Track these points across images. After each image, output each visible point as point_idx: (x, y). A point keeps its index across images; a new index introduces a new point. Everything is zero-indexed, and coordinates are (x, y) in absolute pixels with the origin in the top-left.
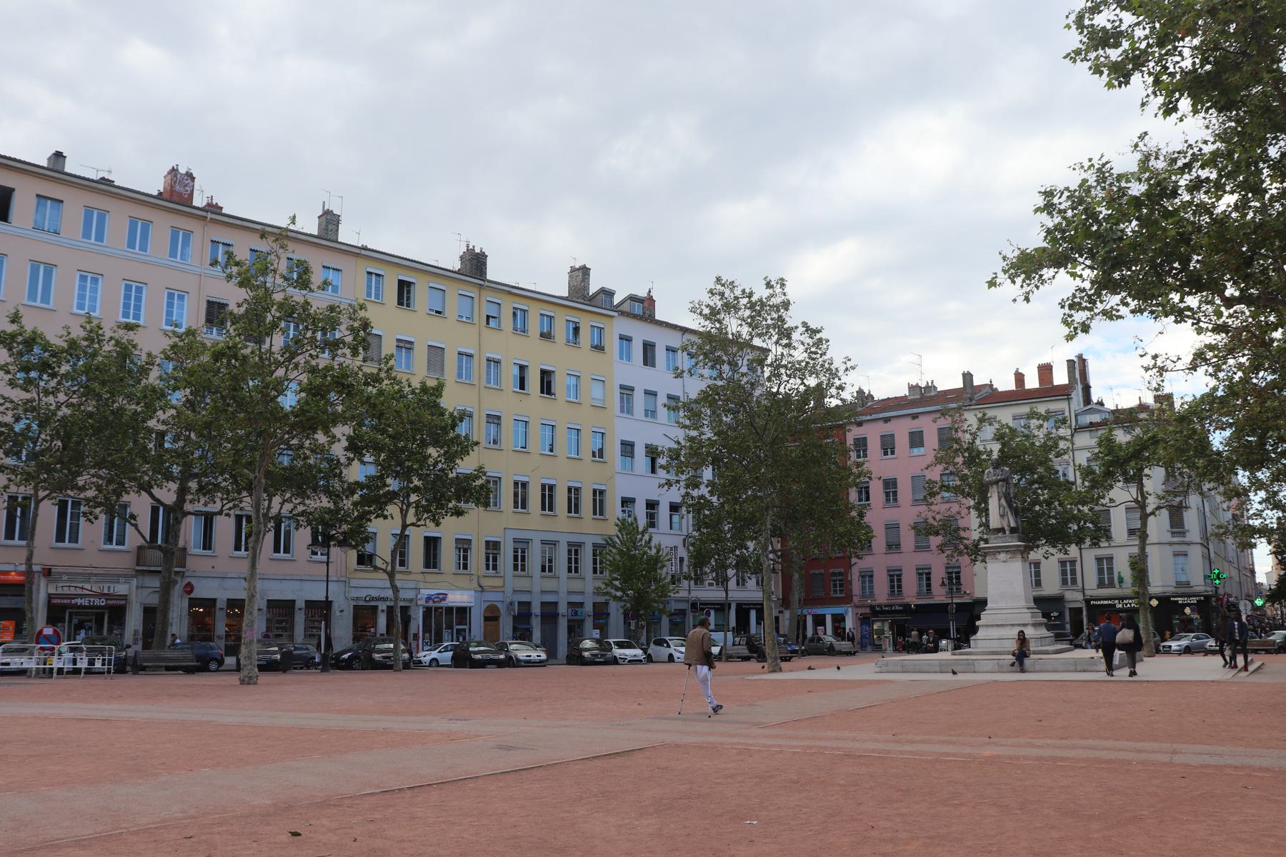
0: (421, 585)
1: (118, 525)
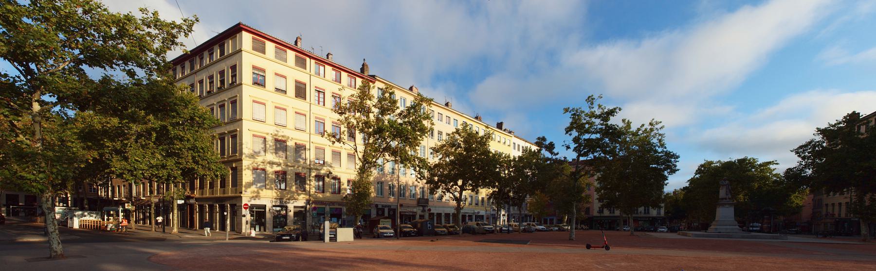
1: (218, 184)
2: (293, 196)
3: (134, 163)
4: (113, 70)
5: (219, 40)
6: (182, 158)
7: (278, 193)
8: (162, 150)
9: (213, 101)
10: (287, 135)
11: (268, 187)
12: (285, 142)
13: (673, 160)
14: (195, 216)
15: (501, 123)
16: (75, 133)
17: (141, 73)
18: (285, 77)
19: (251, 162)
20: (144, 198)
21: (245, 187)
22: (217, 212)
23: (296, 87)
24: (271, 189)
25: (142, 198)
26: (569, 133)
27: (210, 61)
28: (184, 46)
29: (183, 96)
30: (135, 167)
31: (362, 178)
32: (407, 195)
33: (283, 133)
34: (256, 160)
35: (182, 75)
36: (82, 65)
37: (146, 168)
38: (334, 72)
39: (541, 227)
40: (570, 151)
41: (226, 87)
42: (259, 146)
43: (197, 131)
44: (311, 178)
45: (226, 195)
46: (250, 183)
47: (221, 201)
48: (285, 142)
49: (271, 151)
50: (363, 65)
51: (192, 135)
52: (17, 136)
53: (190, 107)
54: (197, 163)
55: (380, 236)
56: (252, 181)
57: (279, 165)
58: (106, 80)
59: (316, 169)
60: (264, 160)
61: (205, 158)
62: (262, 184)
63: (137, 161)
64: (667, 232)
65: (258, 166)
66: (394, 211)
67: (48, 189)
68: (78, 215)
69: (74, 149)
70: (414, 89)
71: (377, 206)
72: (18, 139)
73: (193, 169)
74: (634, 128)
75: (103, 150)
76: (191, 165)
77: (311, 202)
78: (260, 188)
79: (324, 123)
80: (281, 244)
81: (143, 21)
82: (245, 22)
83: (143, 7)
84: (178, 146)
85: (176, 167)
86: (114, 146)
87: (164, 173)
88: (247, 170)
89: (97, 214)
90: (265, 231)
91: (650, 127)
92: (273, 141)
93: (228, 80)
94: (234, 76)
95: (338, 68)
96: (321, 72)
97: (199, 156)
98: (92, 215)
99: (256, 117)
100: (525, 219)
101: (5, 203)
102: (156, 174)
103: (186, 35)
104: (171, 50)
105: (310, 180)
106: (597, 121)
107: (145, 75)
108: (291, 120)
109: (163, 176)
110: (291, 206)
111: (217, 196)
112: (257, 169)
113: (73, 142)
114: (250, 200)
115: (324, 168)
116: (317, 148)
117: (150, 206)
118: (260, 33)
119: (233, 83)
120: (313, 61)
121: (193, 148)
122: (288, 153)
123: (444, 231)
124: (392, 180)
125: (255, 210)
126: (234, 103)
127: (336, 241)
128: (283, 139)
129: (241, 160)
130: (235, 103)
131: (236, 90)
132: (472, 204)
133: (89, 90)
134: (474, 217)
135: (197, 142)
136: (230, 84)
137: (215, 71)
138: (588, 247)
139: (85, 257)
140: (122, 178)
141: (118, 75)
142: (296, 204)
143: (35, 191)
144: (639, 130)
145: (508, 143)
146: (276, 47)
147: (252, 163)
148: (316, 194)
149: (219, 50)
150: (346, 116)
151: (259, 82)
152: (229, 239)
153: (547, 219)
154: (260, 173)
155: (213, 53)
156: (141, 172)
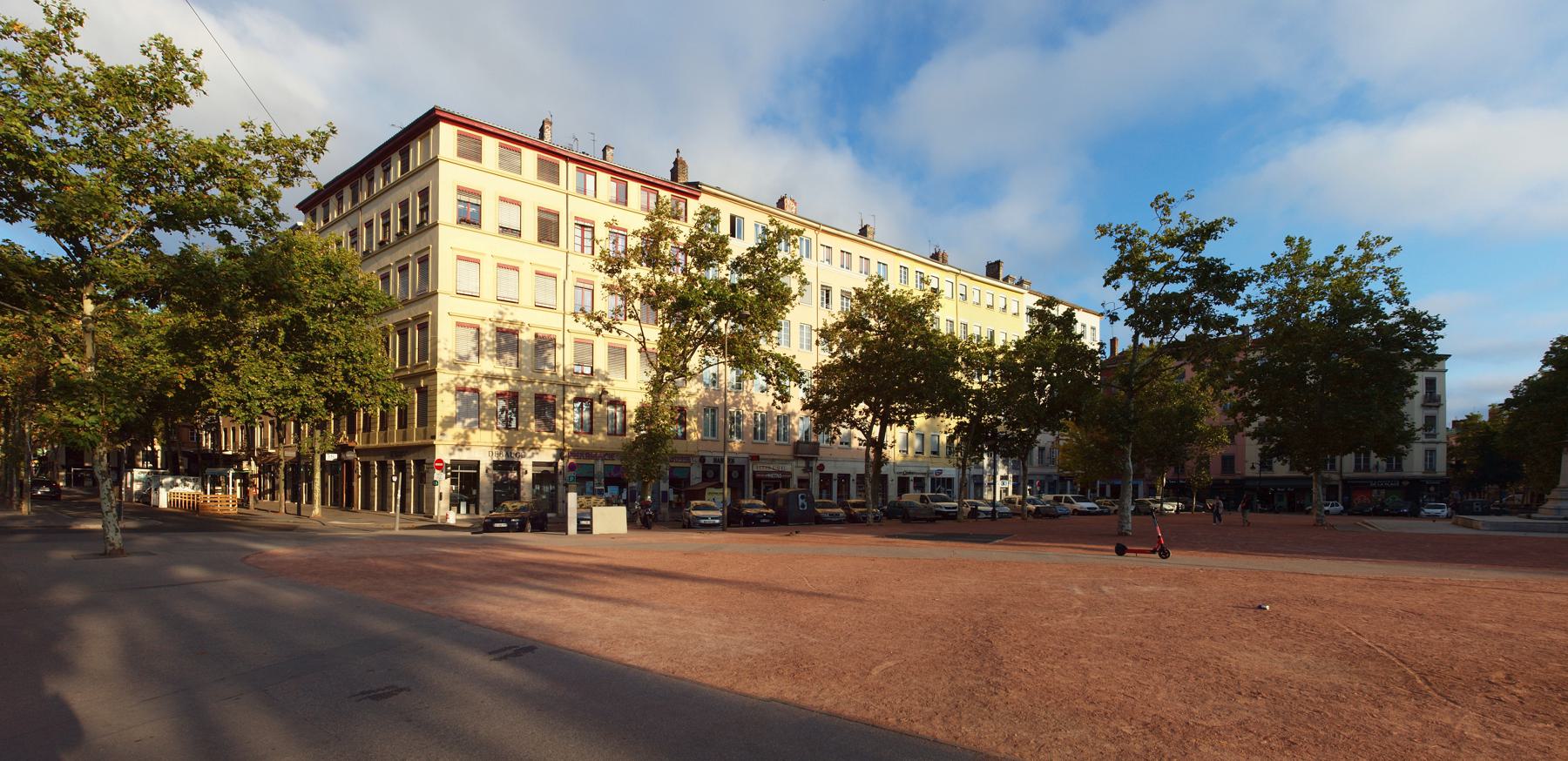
0: (930, 465)
1: (414, 413)
2: (531, 443)
3: (247, 386)
4: (200, 233)
5: (400, 143)
6: (326, 373)
7: (503, 437)
8: (295, 360)
9: (389, 259)
10: (518, 319)
11: (484, 425)
12: (515, 333)
13: (1426, 332)
14: (355, 484)
15: (998, 263)
16: (161, 336)
17: (240, 236)
18: (518, 204)
19: (453, 377)
20: (274, 451)
21: (441, 425)
22: (411, 477)
23: (540, 220)
24: (490, 428)
25: (270, 451)
26: (1113, 283)
27: (384, 184)
28: (314, 177)
29: (330, 257)
30: (248, 395)
31: (656, 401)
32: (770, 435)
33: (513, 315)
34: (462, 372)
35: (338, 214)
36: (154, 231)
37: (268, 395)
38: (614, 184)
39: (1085, 505)
40: (1119, 324)
41: (410, 232)
42: (468, 346)
43: (353, 322)
44: (566, 405)
45: (408, 443)
46: (450, 417)
47: (399, 453)
48: (515, 333)
49: (490, 353)
50: (676, 163)
51: (343, 330)
52: (61, 356)
53: (343, 276)
54: (351, 383)
55: (691, 525)
56: (454, 415)
57: (504, 379)
58: (186, 255)
59: (577, 386)
60: (476, 371)
61: (365, 372)
62: (473, 420)
63: (252, 382)
64: (1341, 513)
65: (466, 383)
66: (741, 469)
67: (103, 441)
68: (167, 484)
69: (158, 366)
70: (787, 202)
71: (702, 459)
72: (63, 361)
73: (345, 394)
74: (1317, 256)
75: (202, 364)
76: (342, 386)
77: (566, 454)
78: (470, 427)
79: (593, 291)
80: (491, 538)
81: (248, 142)
82: (447, 104)
83: (247, 121)
84: (318, 353)
85: (317, 390)
86: (219, 356)
87: (294, 403)
88: (445, 392)
89: (196, 481)
90: (477, 513)
91: (1362, 252)
92: (494, 333)
93: (415, 217)
94: (424, 210)
95: (621, 176)
96: (587, 188)
97: (354, 369)
98: (187, 483)
99: (462, 289)
100: (1059, 487)
101: (64, 463)
102: (283, 406)
103: (316, 158)
104: (293, 186)
105: (564, 409)
106: (1177, 253)
107: (247, 239)
108: (527, 286)
109: (293, 409)
110: (527, 463)
111: (392, 444)
112: (464, 390)
113: (156, 354)
114: (451, 451)
115: (593, 382)
116: (577, 342)
117: (278, 465)
118: (471, 123)
119: (422, 223)
120: (572, 166)
121: (346, 356)
122: (521, 356)
123: (837, 515)
124: (736, 404)
125: (459, 471)
126: (424, 261)
127: (592, 533)
128: (512, 327)
129: (434, 373)
130: (425, 261)
131: (427, 235)
132: (922, 453)
133: (158, 276)
134: (928, 483)
135: (353, 343)
136: (418, 226)
137: (391, 202)
138: (1121, 551)
139: (154, 554)
140: (229, 415)
141: (205, 242)
142: (537, 459)
143: (82, 444)
144: (1330, 261)
145: (1012, 308)
146: (501, 146)
147: (456, 379)
148: (577, 436)
149: (399, 162)
150: (621, 276)
151: (469, 219)
152: (400, 529)
153: (1014, 493)
154: (468, 395)
155: (389, 169)
156: (258, 403)
